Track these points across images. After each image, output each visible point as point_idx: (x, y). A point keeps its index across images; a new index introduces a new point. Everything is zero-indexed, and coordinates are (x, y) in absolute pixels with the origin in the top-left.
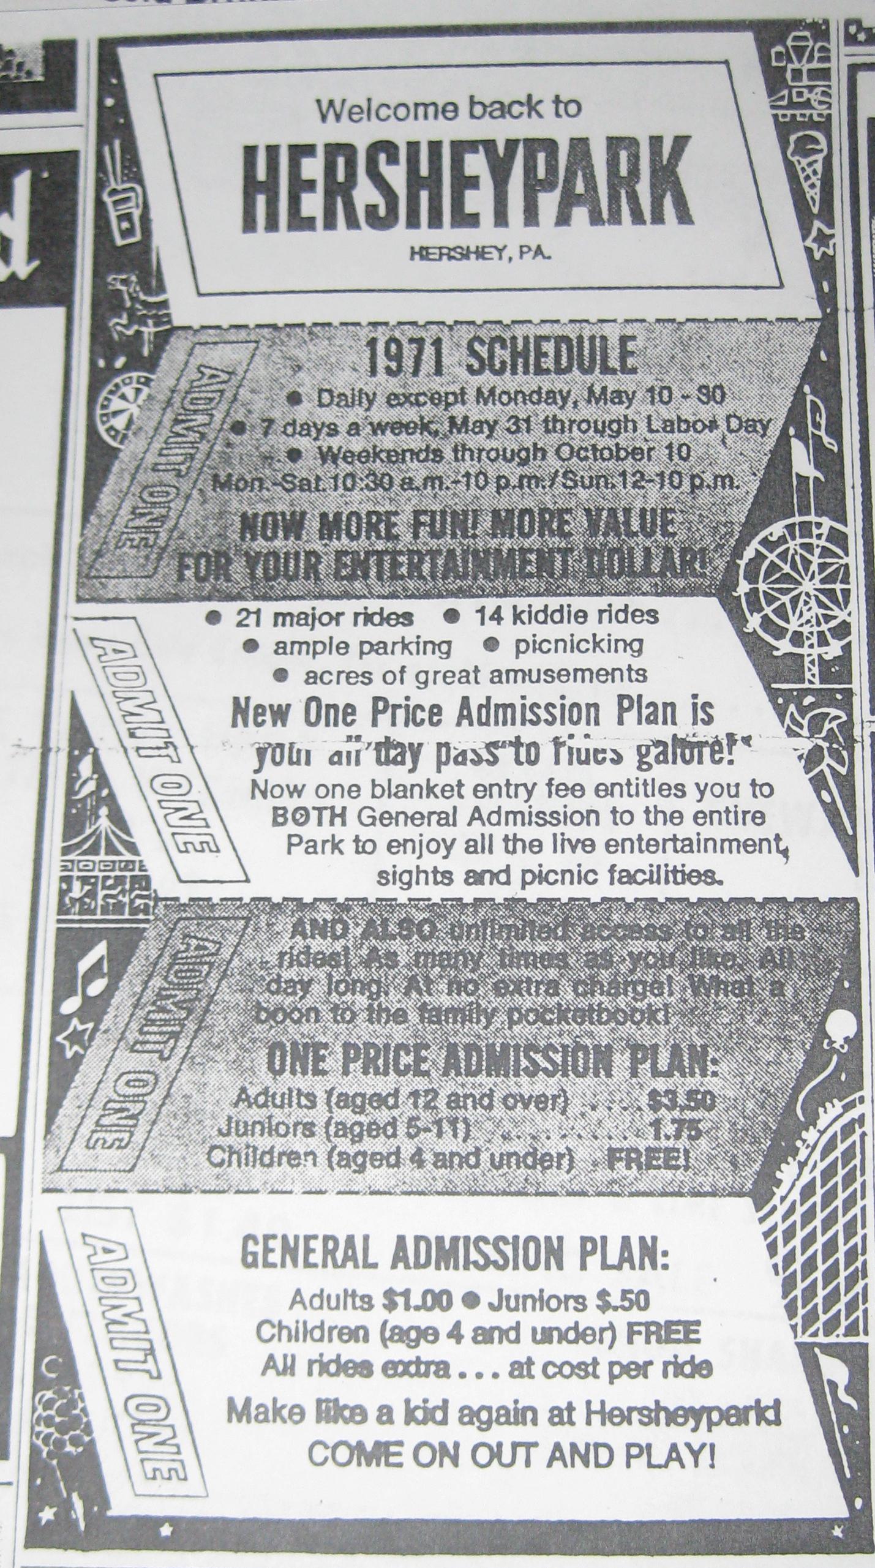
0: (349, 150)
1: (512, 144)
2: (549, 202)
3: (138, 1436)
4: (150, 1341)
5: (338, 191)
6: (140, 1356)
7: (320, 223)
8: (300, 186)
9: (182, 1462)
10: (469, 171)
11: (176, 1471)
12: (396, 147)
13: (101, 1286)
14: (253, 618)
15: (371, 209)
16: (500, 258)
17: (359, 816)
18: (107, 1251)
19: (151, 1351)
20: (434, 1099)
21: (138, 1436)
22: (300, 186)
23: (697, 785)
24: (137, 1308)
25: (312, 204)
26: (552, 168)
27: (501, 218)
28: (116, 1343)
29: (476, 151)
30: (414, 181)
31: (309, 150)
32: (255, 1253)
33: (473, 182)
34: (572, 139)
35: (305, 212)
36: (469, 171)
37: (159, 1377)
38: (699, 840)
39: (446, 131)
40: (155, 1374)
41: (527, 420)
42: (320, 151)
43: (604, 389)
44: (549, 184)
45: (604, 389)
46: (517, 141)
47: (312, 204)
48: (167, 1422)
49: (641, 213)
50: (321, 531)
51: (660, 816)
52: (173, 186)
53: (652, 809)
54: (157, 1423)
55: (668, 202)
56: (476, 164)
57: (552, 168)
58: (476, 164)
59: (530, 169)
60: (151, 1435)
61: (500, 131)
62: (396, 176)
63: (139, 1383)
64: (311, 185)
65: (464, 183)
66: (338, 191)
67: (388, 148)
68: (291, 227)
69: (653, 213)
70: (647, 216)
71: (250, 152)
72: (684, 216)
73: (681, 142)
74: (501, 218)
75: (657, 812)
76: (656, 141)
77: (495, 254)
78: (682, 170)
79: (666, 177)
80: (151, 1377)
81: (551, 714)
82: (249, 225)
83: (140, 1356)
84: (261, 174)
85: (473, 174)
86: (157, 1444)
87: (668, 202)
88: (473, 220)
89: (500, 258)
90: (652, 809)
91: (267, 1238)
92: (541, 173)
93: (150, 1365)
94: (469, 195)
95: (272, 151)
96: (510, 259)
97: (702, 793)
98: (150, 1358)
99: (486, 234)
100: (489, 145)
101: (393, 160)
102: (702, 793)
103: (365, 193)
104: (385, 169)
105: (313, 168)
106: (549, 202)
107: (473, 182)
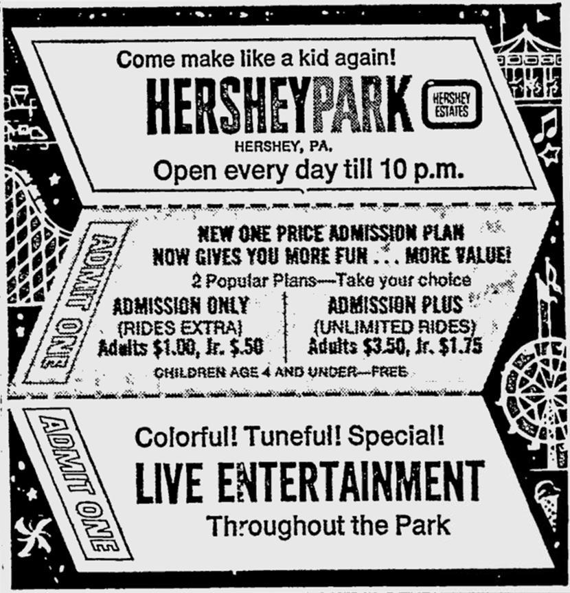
0: (210, 83)
1: (306, 81)
2: (328, 117)
3: (57, 457)
4: (86, 475)
6: (83, 483)
7: (194, 129)
8: (182, 105)
9: (114, 541)
11: (112, 546)
13: (54, 444)
15: (224, 119)
16: (295, 150)
18: (54, 425)
19: (87, 480)
20: (199, 281)
21: (57, 457)
22: (182, 105)
23: (381, 278)
24: (106, 526)
26: (330, 95)
27: (300, 128)
28: (67, 477)
29: (284, 84)
30: (249, 104)
32: (61, 232)
34: (341, 78)
35: (185, 121)
37: (118, 550)
38: (374, 55)
39: (268, 73)
40: (92, 491)
44: (328, 105)
46: (309, 78)
47: (189, 117)
48: (101, 518)
50: (188, 254)
53: (359, 518)
54: (68, 449)
55: (398, 117)
57: (330, 95)
58: (285, 92)
59: (317, 95)
60: (100, 531)
61: (299, 72)
62: (238, 99)
63: (85, 496)
64: (187, 105)
67: (232, 81)
68: (176, 132)
69: (389, 125)
70: (394, 467)
74: (300, 128)
75: (363, 523)
77: (292, 147)
80: (90, 493)
82: (152, 130)
83: (83, 482)
84: (158, 98)
85: (284, 122)
86: (68, 455)
87: (398, 117)
88: (284, 128)
89: (295, 150)
90: (359, 518)
92: (324, 99)
93: (88, 487)
96: (302, 150)
97: (384, 283)
98: (88, 484)
100: (293, 81)
101: (236, 90)
102: (384, 283)
103: (220, 110)
106: (328, 117)
107: (216, 234)
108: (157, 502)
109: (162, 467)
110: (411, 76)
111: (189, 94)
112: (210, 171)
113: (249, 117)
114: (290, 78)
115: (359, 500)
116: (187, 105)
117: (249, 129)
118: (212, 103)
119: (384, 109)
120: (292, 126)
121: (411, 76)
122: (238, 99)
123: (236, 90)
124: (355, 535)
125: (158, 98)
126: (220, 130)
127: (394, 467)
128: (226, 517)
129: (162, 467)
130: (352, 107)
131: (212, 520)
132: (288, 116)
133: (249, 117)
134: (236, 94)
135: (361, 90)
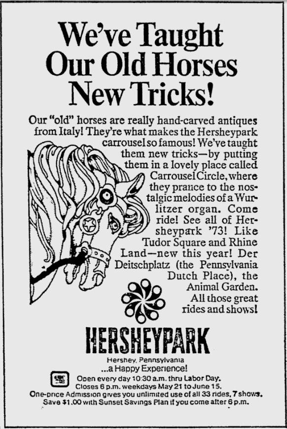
2: (170, 346)
5: (113, 341)
7: (108, 351)
10: (148, 337)
12: (128, 329)
14: (179, 387)
15: (122, 347)
17: (223, 289)
25: (106, 345)
27: (157, 351)
30: (133, 339)
31: (105, 330)
33: (149, 340)
36: (148, 337)
41: (181, 385)
42: (107, 330)
43: (163, 385)
44: (171, 341)
45: (163, 385)
49: (195, 350)
51: (173, 379)
52: (241, 426)
55: (202, 345)
56: (150, 335)
58: (150, 335)
59: (165, 336)
62: (128, 338)
64: (105, 340)
65: (147, 340)
66: (113, 341)
70: (197, 350)
71: (88, 329)
72: (207, 351)
73: (206, 330)
74: (157, 351)
76: (199, 330)
78: (206, 338)
79: (202, 340)
81: (185, 177)
82: (88, 351)
87: (202, 345)
91: (249, 175)
94: (148, 343)
95: (94, 329)
99: (153, 355)
100: (154, 329)
103: (120, 343)
104: (125, 335)
105: (105, 335)
106: (170, 346)
107: (149, 340)
108: (187, 353)
109: (185, 351)
110: (209, 328)
111: (105, 335)
112: (93, 379)
113: (133, 346)
114: (152, 328)
115: (196, 352)
116: (105, 340)
117: (172, 44)
118: (116, 339)
119: (196, 343)
120: (153, 350)
121: (209, 328)
122: (128, 338)
123: (127, 333)
124: (208, 191)
125: (91, 336)
126: (119, 351)
127: (197, 350)
128: (95, 128)
129: (185, 351)
130: (182, 342)
131: (238, 233)
132: (151, 345)
133: (133, 346)
134: (127, 335)
135: (160, 338)
